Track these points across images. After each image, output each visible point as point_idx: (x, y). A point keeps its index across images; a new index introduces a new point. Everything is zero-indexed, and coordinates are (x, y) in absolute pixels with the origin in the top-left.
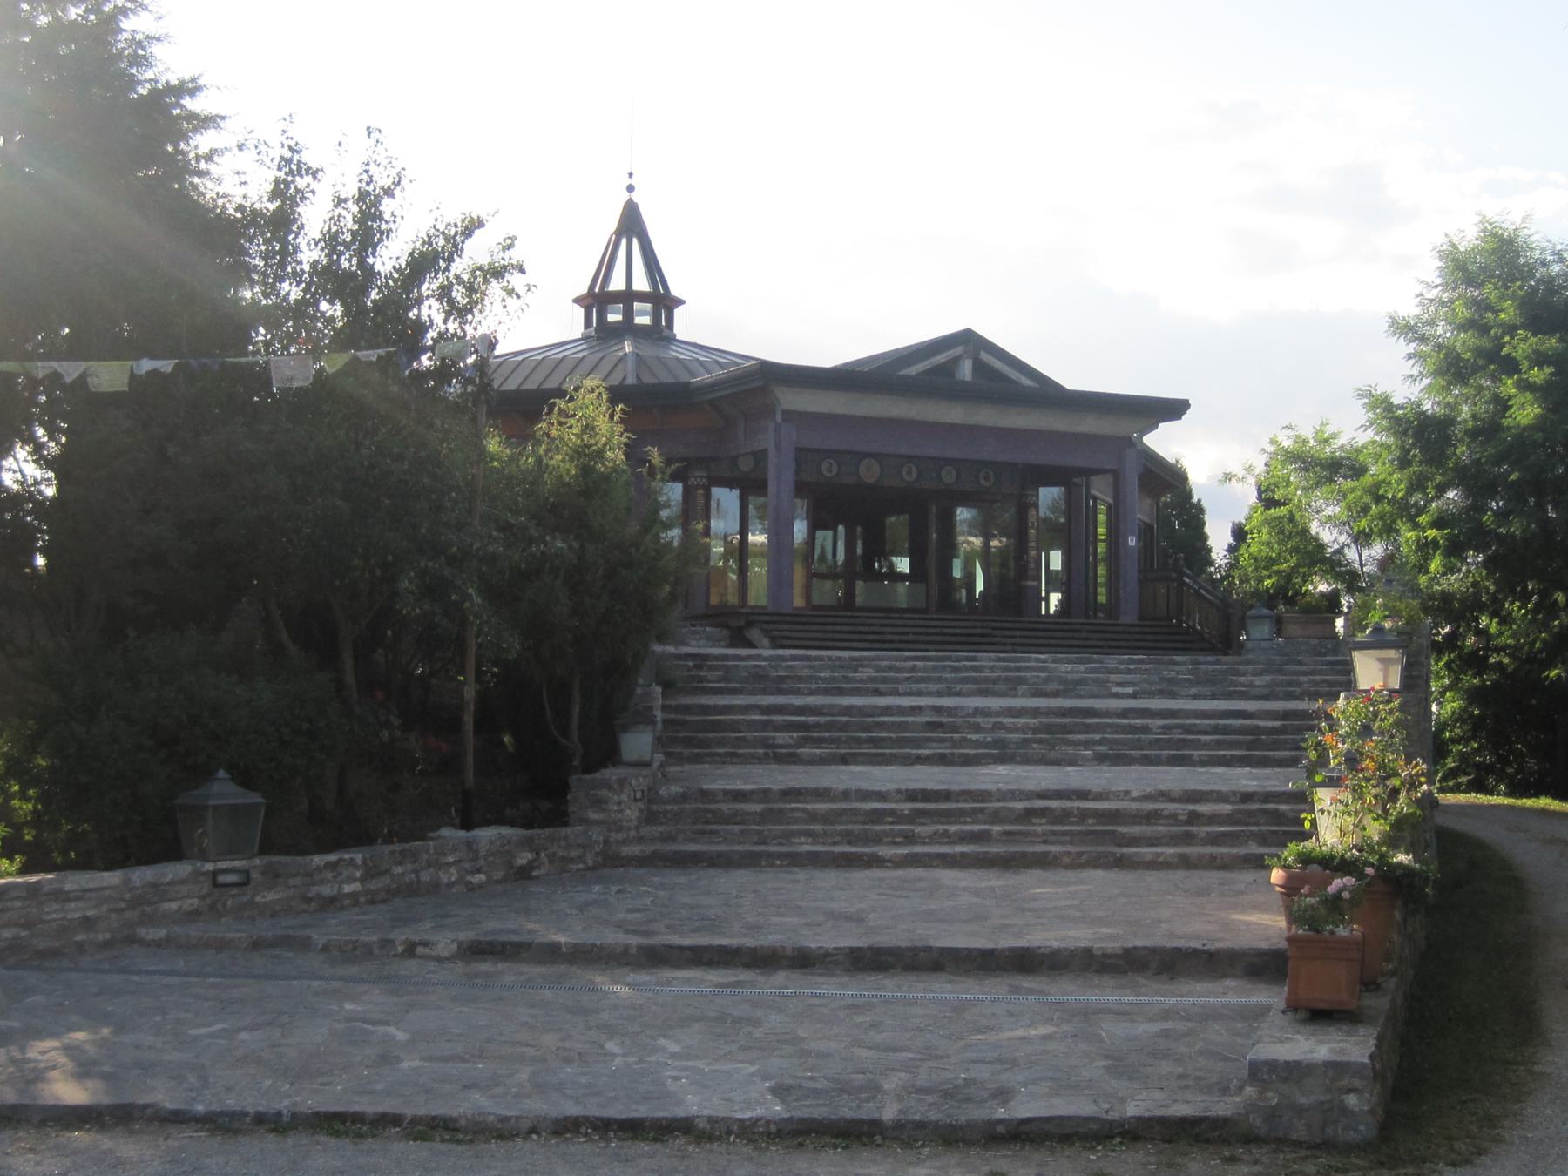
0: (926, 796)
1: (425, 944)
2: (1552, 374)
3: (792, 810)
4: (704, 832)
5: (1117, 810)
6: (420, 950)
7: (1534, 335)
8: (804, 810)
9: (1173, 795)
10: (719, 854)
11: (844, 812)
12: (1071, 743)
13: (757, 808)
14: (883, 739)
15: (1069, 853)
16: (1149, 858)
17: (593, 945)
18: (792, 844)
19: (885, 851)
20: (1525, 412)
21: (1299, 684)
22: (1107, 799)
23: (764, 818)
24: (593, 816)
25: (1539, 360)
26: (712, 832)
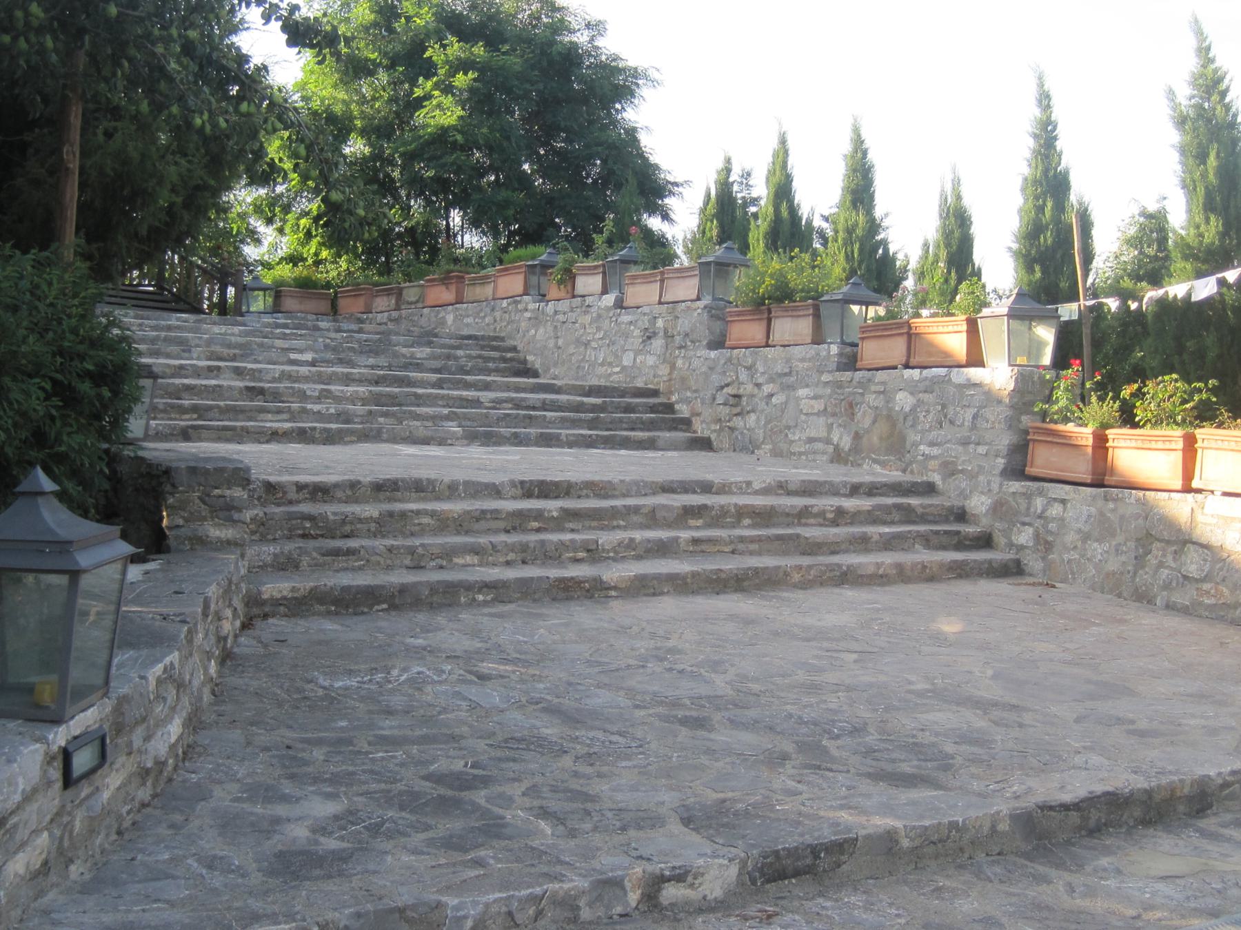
0: (545, 490)
1: (680, 877)
2: (475, 80)
3: (418, 513)
4: (336, 553)
5: (772, 507)
6: (671, 893)
7: (459, 42)
8: (433, 514)
9: (792, 487)
10: (403, 589)
11: (483, 515)
12: (417, 417)
13: (370, 510)
14: (210, 408)
15: (800, 568)
16: (871, 570)
17: (953, 825)
18: (454, 567)
19: (614, 573)
20: (442, 113)
21: (456, 358)
22: (731, 493)
23: (382, 526)
24: (216, 532)
25: (463, 66)
26: (350, 552)
